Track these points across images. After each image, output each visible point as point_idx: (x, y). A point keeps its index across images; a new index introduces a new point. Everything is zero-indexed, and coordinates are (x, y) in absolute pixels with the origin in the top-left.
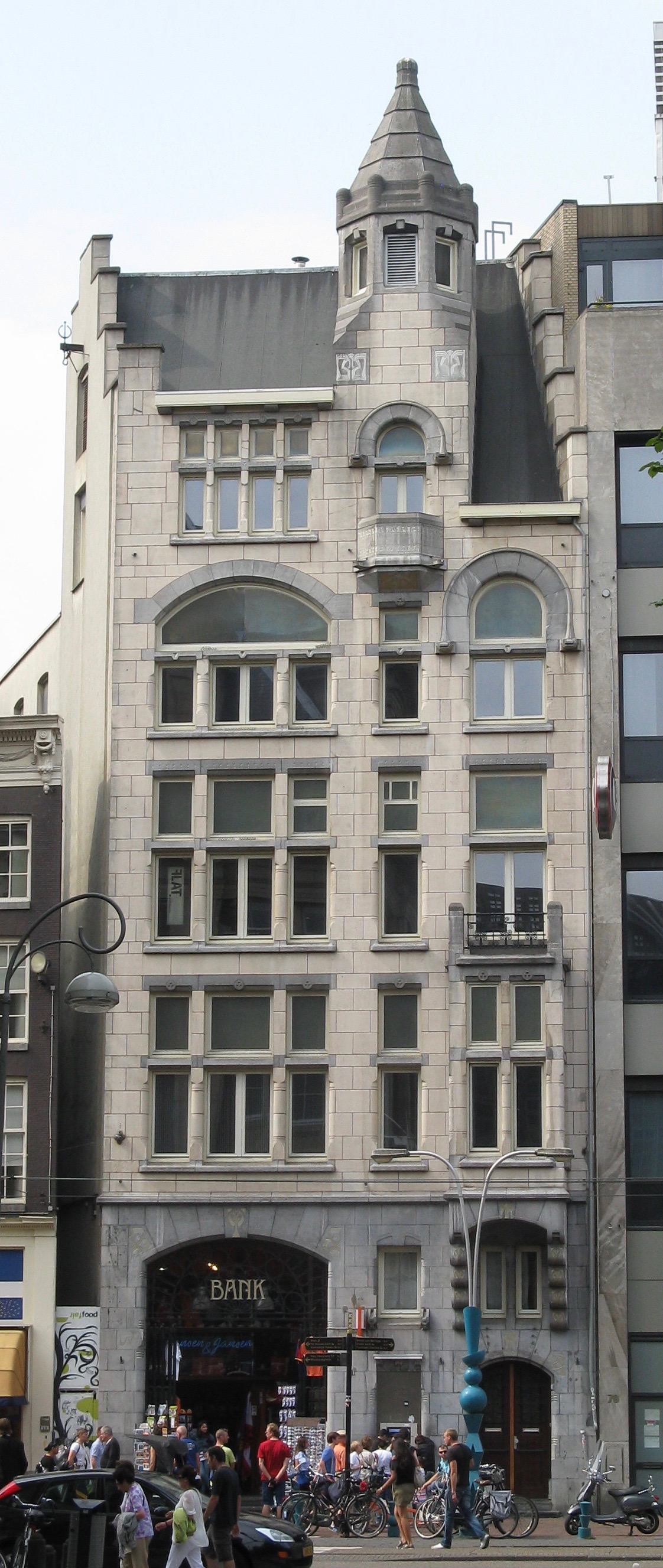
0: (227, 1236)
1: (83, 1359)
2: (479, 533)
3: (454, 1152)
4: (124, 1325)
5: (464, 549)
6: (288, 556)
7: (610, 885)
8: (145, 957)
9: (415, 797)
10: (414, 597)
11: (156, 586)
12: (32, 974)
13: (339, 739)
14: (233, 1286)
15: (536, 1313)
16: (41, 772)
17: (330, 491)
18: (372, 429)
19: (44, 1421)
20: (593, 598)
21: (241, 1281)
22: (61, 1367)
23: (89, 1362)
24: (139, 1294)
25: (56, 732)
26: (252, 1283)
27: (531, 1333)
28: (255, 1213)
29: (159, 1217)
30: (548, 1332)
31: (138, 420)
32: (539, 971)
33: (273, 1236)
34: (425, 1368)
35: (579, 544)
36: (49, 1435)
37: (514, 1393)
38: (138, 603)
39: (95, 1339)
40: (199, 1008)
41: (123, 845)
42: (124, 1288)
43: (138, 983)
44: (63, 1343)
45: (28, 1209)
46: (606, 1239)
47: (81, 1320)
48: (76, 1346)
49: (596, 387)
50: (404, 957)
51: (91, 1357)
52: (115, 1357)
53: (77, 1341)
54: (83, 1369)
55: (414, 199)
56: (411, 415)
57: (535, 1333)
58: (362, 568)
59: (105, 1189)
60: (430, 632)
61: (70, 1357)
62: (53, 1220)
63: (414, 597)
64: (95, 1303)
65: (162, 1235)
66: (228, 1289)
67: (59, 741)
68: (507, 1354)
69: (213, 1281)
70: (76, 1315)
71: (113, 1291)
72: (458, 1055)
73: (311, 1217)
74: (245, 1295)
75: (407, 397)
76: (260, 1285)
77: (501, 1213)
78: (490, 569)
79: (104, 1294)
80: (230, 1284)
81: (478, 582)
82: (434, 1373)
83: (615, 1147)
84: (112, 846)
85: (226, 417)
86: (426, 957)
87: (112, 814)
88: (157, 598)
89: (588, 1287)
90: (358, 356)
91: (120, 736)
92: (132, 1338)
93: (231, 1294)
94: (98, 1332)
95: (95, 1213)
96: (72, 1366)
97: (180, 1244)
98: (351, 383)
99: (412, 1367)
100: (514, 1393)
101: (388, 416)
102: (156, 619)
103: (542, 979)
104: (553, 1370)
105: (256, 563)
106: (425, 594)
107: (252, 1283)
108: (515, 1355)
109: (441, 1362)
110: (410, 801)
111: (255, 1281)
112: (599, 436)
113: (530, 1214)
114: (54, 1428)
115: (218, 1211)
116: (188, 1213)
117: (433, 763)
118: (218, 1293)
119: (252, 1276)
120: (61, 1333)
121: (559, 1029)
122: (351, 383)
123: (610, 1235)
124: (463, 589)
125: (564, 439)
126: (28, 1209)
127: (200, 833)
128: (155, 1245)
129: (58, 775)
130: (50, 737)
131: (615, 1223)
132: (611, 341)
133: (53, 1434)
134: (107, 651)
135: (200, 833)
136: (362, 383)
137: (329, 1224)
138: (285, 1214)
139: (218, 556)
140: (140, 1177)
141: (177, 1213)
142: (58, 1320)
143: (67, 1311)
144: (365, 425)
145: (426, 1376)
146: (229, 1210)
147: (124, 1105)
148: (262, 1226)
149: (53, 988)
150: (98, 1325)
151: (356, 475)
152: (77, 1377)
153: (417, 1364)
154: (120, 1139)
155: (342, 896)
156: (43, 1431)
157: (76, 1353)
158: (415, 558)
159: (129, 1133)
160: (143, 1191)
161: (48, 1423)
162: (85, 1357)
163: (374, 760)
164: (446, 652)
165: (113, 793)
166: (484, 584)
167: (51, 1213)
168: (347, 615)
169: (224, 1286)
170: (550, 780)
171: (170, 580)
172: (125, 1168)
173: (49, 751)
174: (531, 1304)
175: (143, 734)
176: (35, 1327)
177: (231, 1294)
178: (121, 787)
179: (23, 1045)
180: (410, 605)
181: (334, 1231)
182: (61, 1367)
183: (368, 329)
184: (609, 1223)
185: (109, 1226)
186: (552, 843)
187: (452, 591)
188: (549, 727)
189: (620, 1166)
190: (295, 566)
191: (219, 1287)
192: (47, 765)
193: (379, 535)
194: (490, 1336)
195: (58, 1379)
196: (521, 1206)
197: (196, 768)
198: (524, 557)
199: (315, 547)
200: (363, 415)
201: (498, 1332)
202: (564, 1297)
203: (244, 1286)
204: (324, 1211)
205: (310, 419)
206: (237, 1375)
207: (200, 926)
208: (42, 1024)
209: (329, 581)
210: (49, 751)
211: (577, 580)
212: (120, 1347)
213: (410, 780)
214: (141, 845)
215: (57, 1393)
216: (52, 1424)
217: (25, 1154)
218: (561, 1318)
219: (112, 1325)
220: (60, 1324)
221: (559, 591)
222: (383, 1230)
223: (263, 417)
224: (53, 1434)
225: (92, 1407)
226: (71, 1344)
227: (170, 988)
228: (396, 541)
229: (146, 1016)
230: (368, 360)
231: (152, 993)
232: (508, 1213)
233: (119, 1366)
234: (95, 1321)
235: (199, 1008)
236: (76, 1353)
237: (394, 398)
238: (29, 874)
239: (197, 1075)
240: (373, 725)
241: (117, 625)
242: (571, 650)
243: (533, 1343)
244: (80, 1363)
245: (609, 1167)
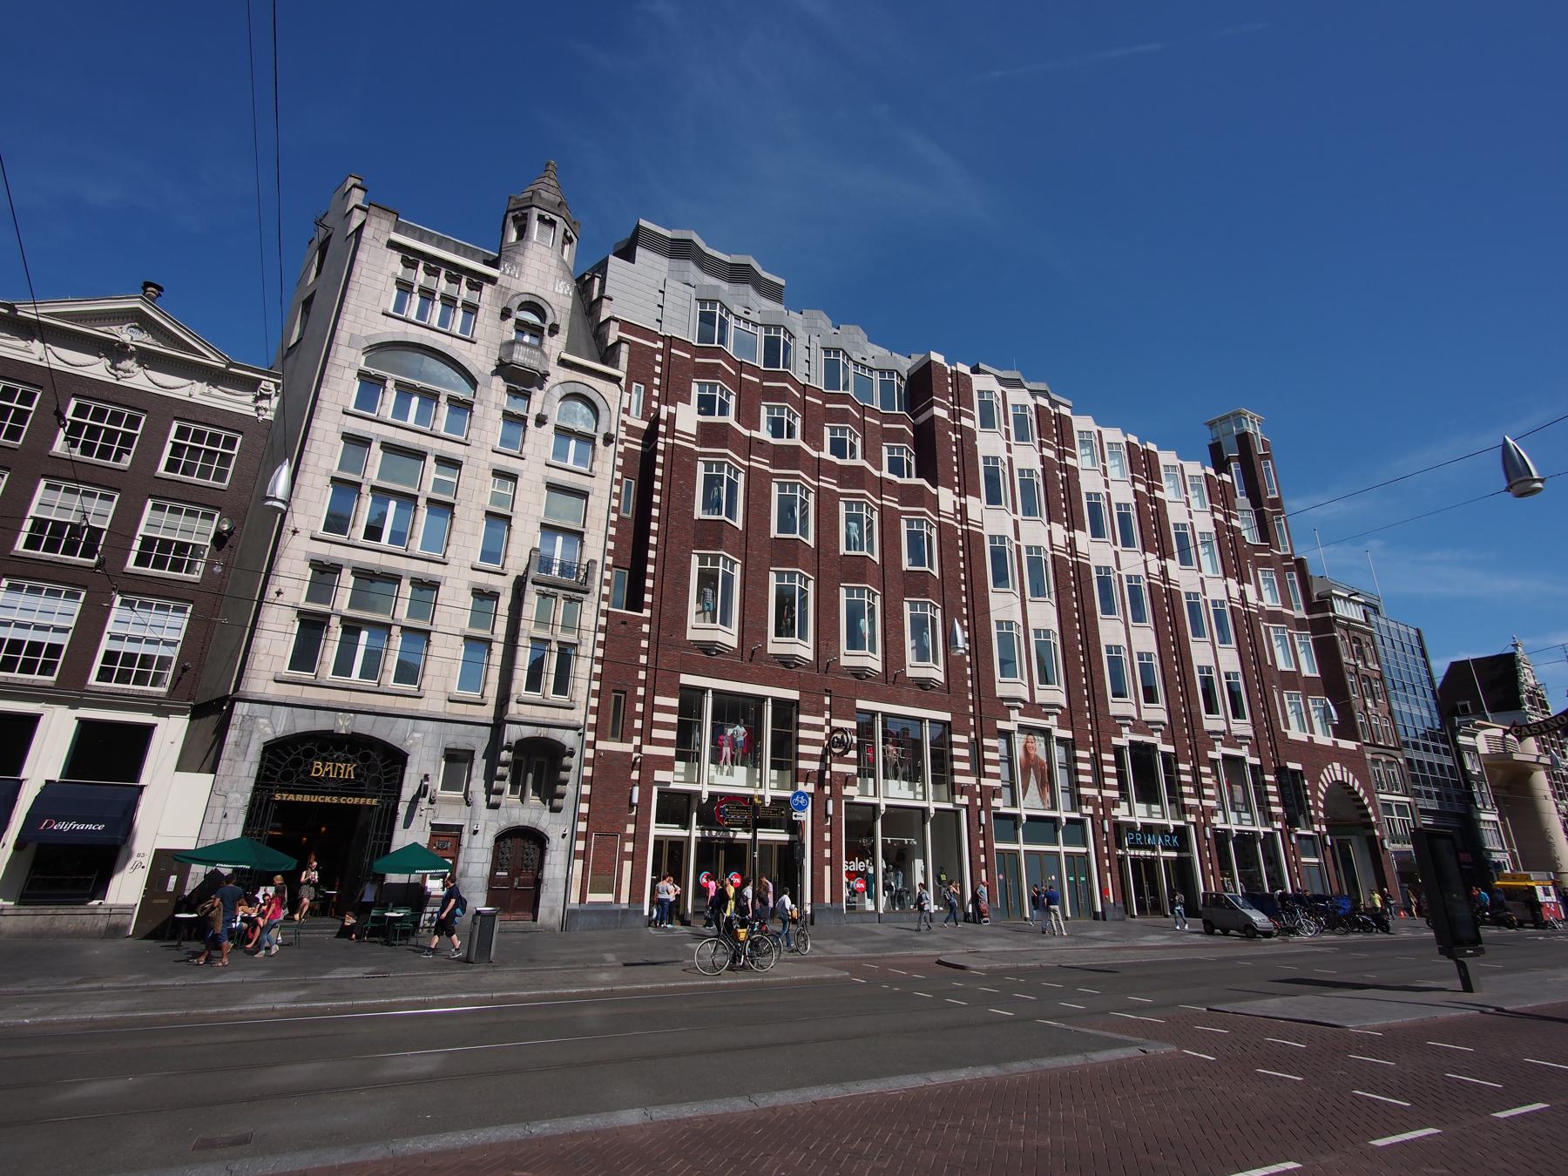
18: (517, 302)
31: (373, 243)
41: (309, 469)
56: (540, 302)
65: (279, 724)
78: (572, 389)
85: (434, 266)
101: (527, 298)
118: (317, 771)
119: (347, 761)
127: (342, 601)
135: (342, 601)
137: (414, 730)
148: (364, 726)
183: (514, 263)
200: (511, 293)
207: (358, 533)
223: (456, 273)
238: (231, 469)
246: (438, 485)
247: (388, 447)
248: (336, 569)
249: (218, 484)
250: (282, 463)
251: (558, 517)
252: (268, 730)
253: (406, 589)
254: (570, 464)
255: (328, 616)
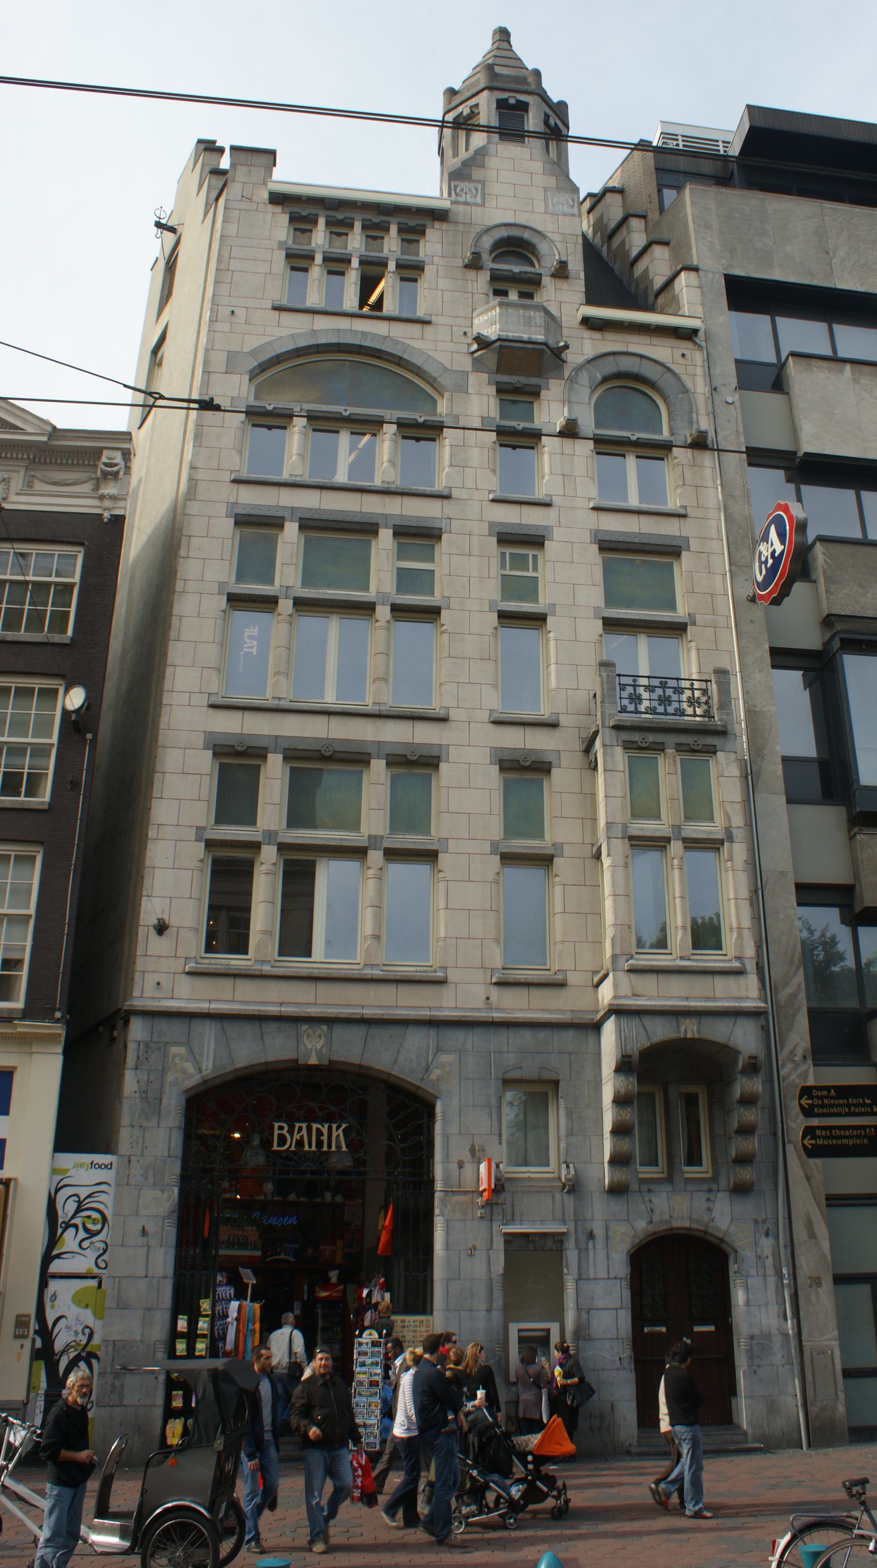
0: (301, 1062)
1: (86, 1230)
2: (597, 335)
3: (618, 951)
4: (151, 1180)
5: (584, 347)
6: (398, 331)
7: (760, 671)
8: (211, 711)
9: (535, 569)
10: (533, 381)
11: (252, 342)
12: (65, 713)
13: (452, 502)
14: (304, 1132)
15: (705, 1169)
16: (102, 498)
17: (443, 283)
18: (487, 242)
19: (21, 1322)
20: (716, 403)
21: (315, 1126)
22: (53, 1240)
23: (92, 1234)
24: (174, 1137)
25: (127, 455)
26: (330, 1128)
27: (705, 1196)
28: (339, 1032)
29: (208, 1032)
30: (728, 1194)
31: (245, 205)
32: (709, 740)
33: (364, 1063)
34: (570, 1244)
35: (698, 357)
36: (28, 1343)
37: (681, 1279)
38: (232, 358)
39: (107, 1202)
40: (274, 781)
41: (192, 586)
42: (151, 1136)
43: (200, 740)
44: (59, 1207)
45: (27, 1014)
46: (789, 1074)
47: (85, 1171)
48: (78, 1210)
49: (703, 238)
50: (529, 731)
51: (99, 1227)
52: (135, 1226)
53: (80, 1203)
54: (85, 1244)
55: (510, 106)
56: (526, 235)
57: (712, 1196)
58: (482, 342)
59: (136, 993)
60: (550, 413)
61: (67, 1225)
62: (60, 1030)
63: (533, 381)
64: (107, 1148)
65: (201, 1060)
66: (296, 1136)
67: (128, 469)
68: (676, 1224)
69: (276, 1125)
70: (81, 1165)
71: (137, 1132)
72: (618, 831)
73: (416, 1042)
74: (320, 1144)
75: (522, 220)
76: (340, 1131)
77: (682, 1029)
78: (611, 366)
79: (125, 1136)
80: (300, 1129)
81: (599, 377)
82: (582, 1252)
83: (791, 961)
84: (179, 585)
86: (557, 733)
87: (183, 553)
88: (253, 353)
89: (775, 1135)
90: (472, 185)
91: (200, 475)
92: (160, 1202)
93: (300, 1143)
94: (111, 1190)
95: (115, 1034)
96: (70, 1240)
97: (236, 1070)
98: (466, 203)
99: (550, 1243)
100: (681, 1279)
101: (504, 233)
102: (251, 372)
103: (712, 751)
104: (737, 1244)
105: (364, 334)
106: (544, 380)
107: (330, 1128)
108: (687, 1224)
109: (591, 1236)
110: (531, 574)
111: (334, 1126)
112: (710, 276)
113: (718, 1032)
114: (36, 1332)
115: (289, 1027)
116: (249, 1030)
117: (557, 533)
118: (282, 1140)
119: (329, 1119)
120: (57, 1190)
121: (738, 807)
122: (466, 203)
123: (795, 1069)
124: (584, 378)
125: (669, 283)
126: (27, 1014)
128: (200, 1071)
129: (121, 504)
130: (118, 458)
131: (800, 1052)
132: (714, 207)
133: (34, 1340)
134: (196, 350)
136: (477, 205)
137: (438, 1050)
138: (381, 1034)
139: (323, 323)
140: (185, 980)
141: (233, 1029)
142: (54, 1171)
143: (69, 1160)
144: (479, 236)
145: (571, 1255)
146: (305, 1027)
147: (171, 885)
148: (350, 1049)
149: (89, 736)
150: (112, 1181)
151: (471, 274)
152: (77, 1256)
153: (559, 1239)
154: (161, 928)
155: (456, 660)
156: (16, 1337)
157: (78, 1221)
158: (540, 338)
159: (173, 922)
160: (188, 996)
161: (26, 1325)
162: (90, 1226)
163: (492, 525)
164: (570, 431)
165: (185, 532)
166: (605, 380)
167: (58, 1021)
168: (462, 388)
169: (291, 1132)
170: (683, 570)
171: (269, 339)
172: (165, 968)
173: (117, 474)
174: (694, 1158)
175: (227, 477)
176: (21, 1180)
177: (300, 1143)
178: (196, 526)
179: (43, 803)
180: (528, 389)
181: (444, 1058)
182: (53, 1240)
184: (792, 1053)
185: (139, 1043)
186: (694, 623)
187: (572, 380)
188: (682, 511)
189: (799, 985)
190: (407, 341)
191: (285, 1132)
192: (110, 489)
193: (501, 314)
194: (654, 1200)
195: (48, 1258)
196: (706, 1021)
197: (287, 514)
198: (644, 361)
199: (427, 328)
200: (475, 230)
201: (664, 1195)
202: (752, 1144)
203: (320, 1133)
204: (433, 1032)
205: (425, 226)
206: (281, 1260)
208: (70, 779)
209: (443, 358)
210: (117, 474)
211: (700, 387)
212: (143, 1212)
213: (530, 552)
214: (215, 588)
215: (45, 1278)
216: (33, 1325)
217: (29, 943)
218: (746, 1174)
219: (132, 1181)
220: (57, 1178)
221: (682, 393)
222: (510, 1059)
224: (34, 1340)
225: (94, 1301)
226: (72, 1206)
227: (239, 749)
228: (519, 322)
229: (206, 780)
230: (483, 189)
231: (216, 755)
232: (690, 1029)
233: (141, 1240)
234: (106, 1175)
235: (274, 781)
236: (78, 1221)
237: (510, 220)
238: (73, 610)
239: (269, 855)
240: (490, 492)
241: (206, 372)
242: (700, 443)
243: (709, 1209)
244: (82, 1234)
245: (786, 984)
246: (405, 579)
247: (311, 525)
248: (272, 523)
249: (56, 638)
250: (399, 1507)
251: (630, 603)
252: (190, 1067)
253: (377, 779)
254: (633, 501)
255: (255, 846)
